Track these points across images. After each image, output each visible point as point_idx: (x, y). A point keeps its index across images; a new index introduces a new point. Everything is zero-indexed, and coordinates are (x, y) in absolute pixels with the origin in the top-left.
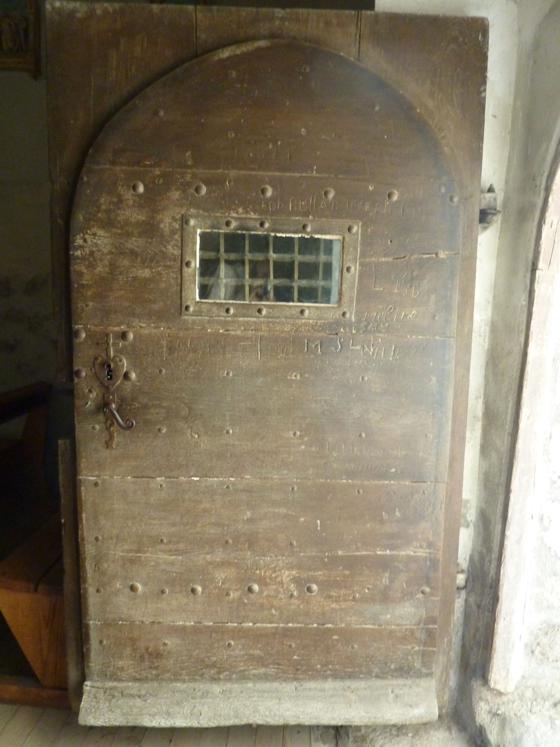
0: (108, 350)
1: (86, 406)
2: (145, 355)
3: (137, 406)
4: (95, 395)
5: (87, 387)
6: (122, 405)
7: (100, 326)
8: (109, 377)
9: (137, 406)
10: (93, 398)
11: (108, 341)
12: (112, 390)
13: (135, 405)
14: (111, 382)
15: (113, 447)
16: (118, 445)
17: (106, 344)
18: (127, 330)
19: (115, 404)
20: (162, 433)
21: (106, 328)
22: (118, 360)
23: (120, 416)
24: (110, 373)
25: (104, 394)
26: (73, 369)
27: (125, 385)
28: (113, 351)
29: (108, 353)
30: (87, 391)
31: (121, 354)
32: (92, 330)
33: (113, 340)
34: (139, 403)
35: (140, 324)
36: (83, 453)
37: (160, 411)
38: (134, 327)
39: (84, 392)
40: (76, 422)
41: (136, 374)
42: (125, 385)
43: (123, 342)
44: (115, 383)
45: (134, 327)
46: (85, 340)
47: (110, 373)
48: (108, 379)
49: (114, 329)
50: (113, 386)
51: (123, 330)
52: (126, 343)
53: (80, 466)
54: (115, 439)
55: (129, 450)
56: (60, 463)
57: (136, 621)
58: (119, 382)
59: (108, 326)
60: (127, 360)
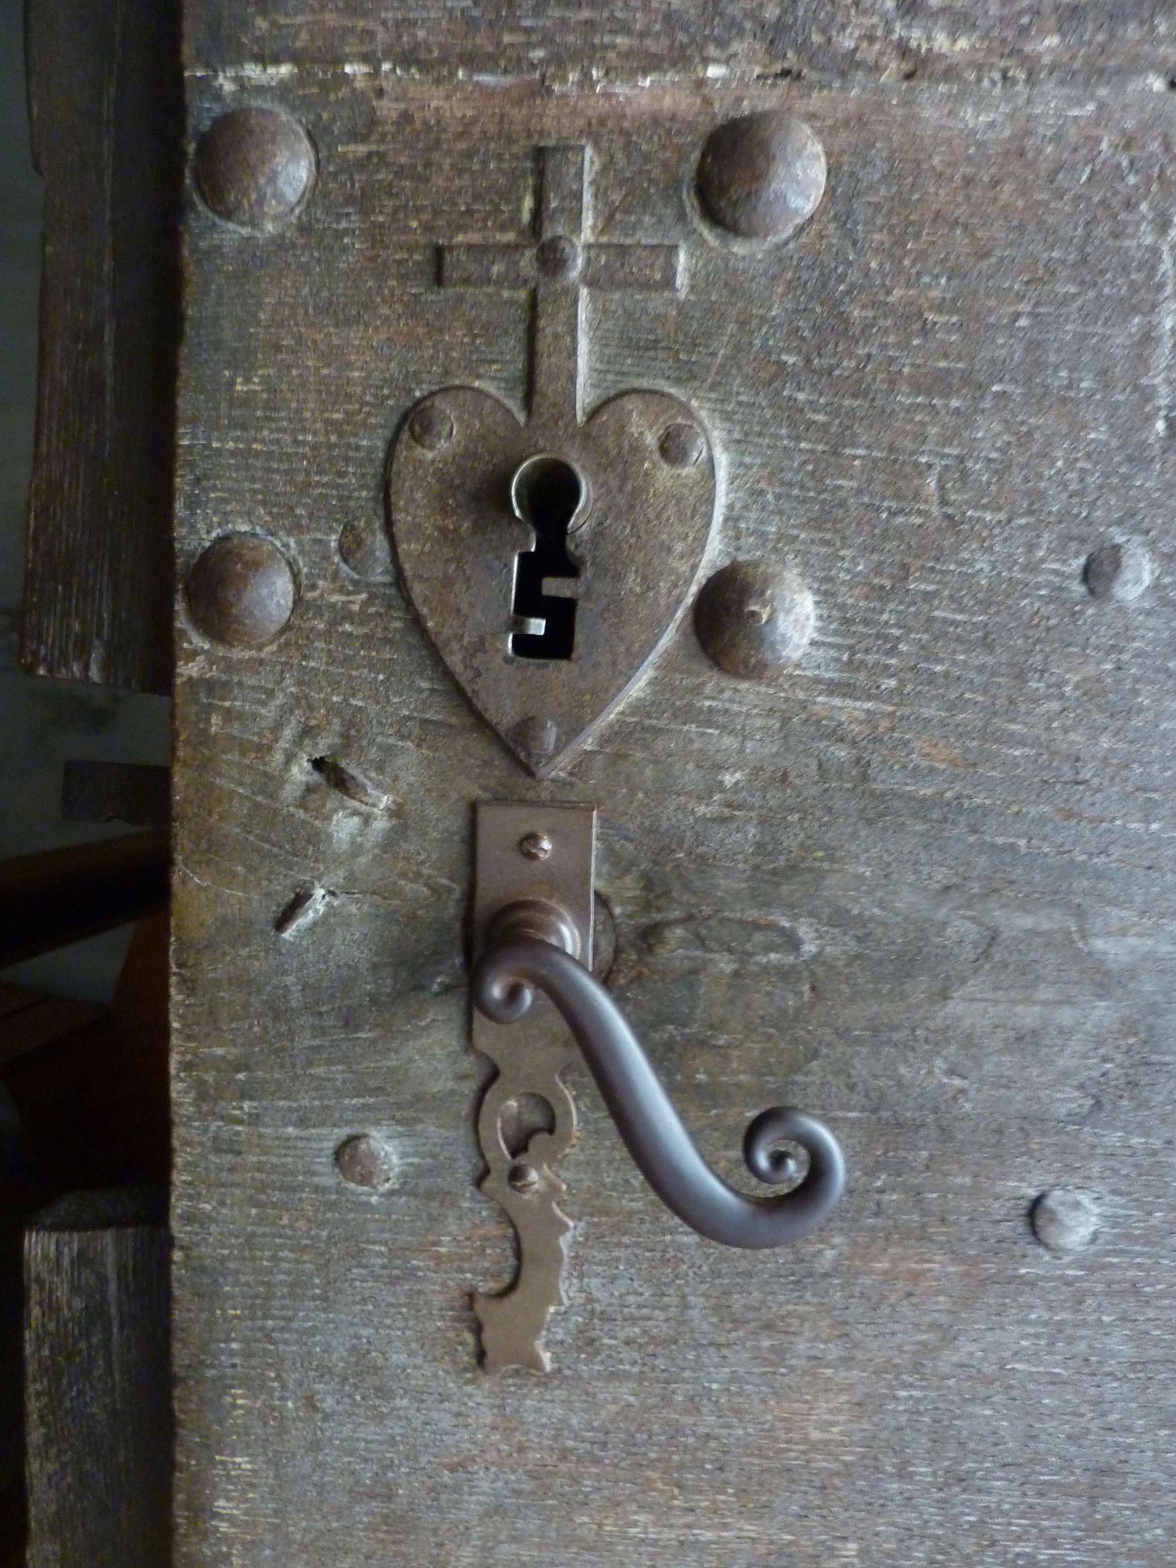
0: (547, 327)
1: (288, 934)
2: (940, 383)
3: (810, 948)
4: (381, 824)
5: (307, 732)
6: (649, 936)
7: (474, 61)
8: (537, 626)
9: (810, 948)
10: (356, 850)
11: (554, 229)
12: (559, 768)
13: (793, 943)
14: (557, 672)
15: (534, 1363)
16: (587, 1343)
17: (527, 261)
18: (767, 99)
19: (581, 921)
20: (1056, 1252)
21: (542, 89)
22: (651, 439)
23: (672, 1090)
24: (552, 586)
25: (473, 808)
26: (392, 829)
27: (708, 718)
28: (600, 340)
29: (545, 364)
30: (300, 773)
31: (688, 375)
32: (388, 108)
33: (608, 222)
34: (839, 918)
35: (916, 37)
36: (240, 1398)
37: (1065, 1016)
38: (849, 65)
39: (270, 783)
40: (178, 1089)
41: (826, 597)
42: (708, 718)
43: (709, 236)
44: (601, 698)
45: (849, 65)
46: (305, 229)
47: (552, 586)
48: (526, 646)
49: (621, 89)
50: (573, 730)
51: (722, 110)
52: (739, 248)
53: (201, 1511)
54: (568, 1289)
55: (693, 1405)
56: (35, 1436)
57: (444, 1021)
58: (638, 686)
59: (559, 61)
60: (737, 445)
